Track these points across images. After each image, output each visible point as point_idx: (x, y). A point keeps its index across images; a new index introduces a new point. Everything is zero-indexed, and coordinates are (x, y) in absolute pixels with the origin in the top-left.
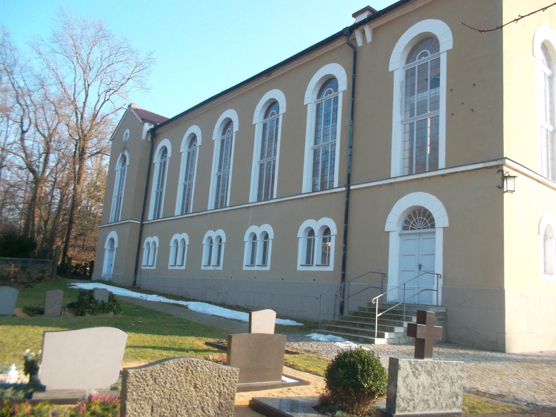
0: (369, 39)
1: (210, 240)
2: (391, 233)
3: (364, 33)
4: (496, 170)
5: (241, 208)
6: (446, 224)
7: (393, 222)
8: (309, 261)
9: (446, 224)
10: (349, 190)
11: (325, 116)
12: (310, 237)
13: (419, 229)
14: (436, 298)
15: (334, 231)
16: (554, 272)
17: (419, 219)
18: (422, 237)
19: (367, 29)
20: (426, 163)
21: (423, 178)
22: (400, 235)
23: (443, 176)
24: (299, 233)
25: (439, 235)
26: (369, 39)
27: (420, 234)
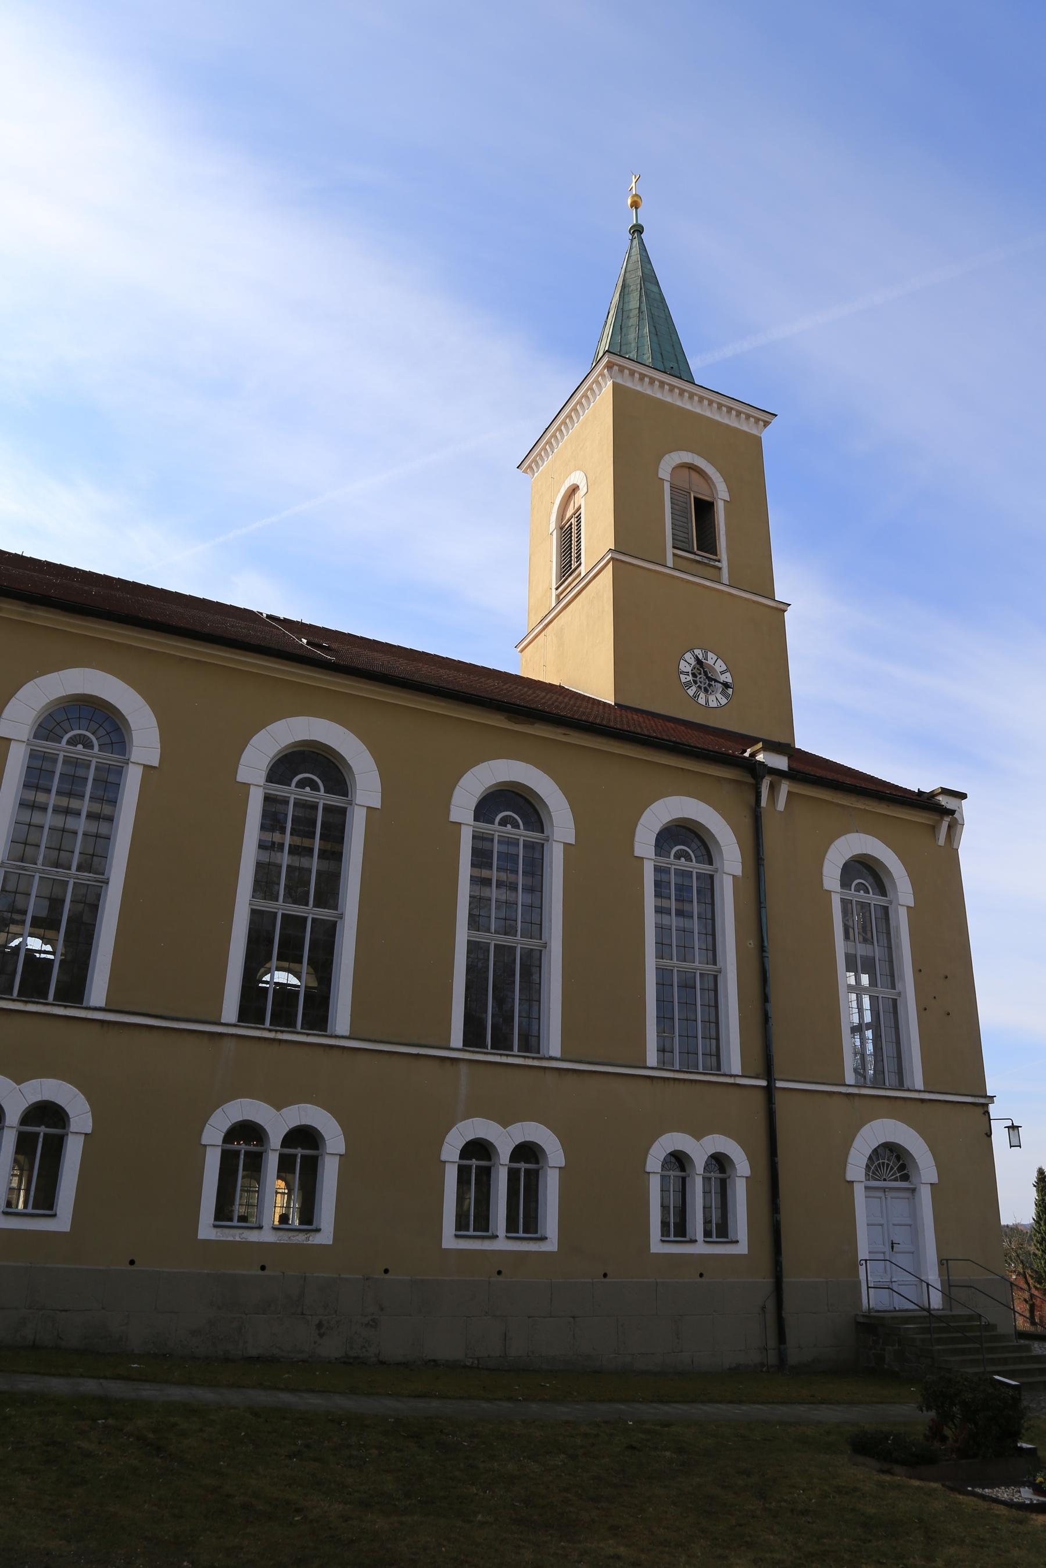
0: (781, 805)
1: (679, 1160)
2: (855, 1184)
3: (773, 788)
4: (981, 1110)
5: (331, 1047)
6: (935, 1179)
7: (856, 1168)
8: (677, 1227)
9: (935, 1179)
10: (769, 1091)
11: (689, 899)
12: (515, 1165)
13: (885, 1180)
14: (936, 1301)
15: (742, 1165)
16: (606, 1280)
17: (891, 1161)
18: (889, 1195)
19: (785, 787)
20: (513, 1012)
21: (896, 1098)
22: (867, 1188)
23: (922, 1101)
24: (849, 1167)
25: (925, 1195)
26: (781, 805)
27: (884, 1190)
